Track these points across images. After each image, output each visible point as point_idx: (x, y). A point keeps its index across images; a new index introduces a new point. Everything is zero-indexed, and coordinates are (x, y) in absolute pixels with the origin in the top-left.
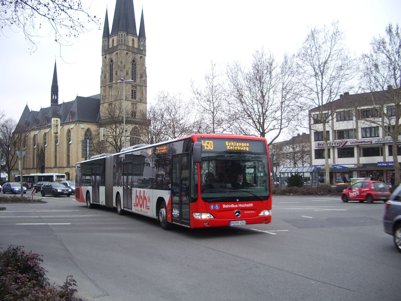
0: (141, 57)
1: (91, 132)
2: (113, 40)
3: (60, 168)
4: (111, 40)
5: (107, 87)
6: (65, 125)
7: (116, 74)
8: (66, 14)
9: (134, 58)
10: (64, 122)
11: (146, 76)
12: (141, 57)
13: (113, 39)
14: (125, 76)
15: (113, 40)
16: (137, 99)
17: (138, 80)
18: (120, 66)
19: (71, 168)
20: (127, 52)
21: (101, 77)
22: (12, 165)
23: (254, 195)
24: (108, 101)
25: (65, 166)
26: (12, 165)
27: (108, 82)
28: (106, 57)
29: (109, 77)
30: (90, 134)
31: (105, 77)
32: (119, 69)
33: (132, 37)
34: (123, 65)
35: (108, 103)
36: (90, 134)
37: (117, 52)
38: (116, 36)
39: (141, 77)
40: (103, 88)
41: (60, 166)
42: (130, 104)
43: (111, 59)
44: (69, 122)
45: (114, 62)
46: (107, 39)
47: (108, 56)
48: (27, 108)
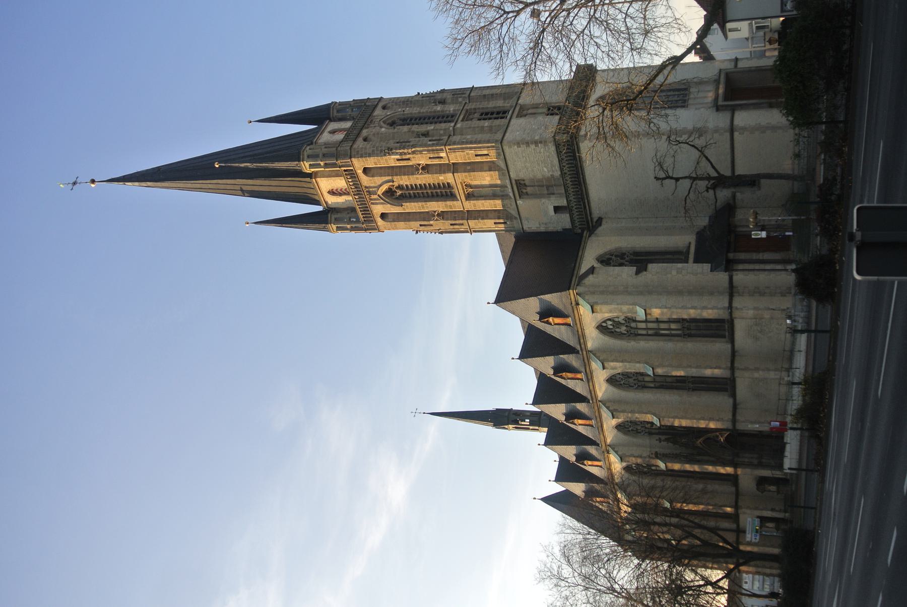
1: (612, 255)
2: (332, 192)
3: (736, 365)
4: (332, 200)
9: (384, 122)
11: (443, 91)
12: (384, 108)
13: (329, 192)
14: (430, 138)
15: (332, 192)
17: (451, 108)
18: (398, 157)
19: (736, 314)
20: (360, 139)
23: (751, 593)
24: (510, 197)
25: (729, 346)
34: (398, 144)
35: (518, 197)
39: (443, 102)
41: (729, 365)
42: (522, 121)
46: (333, 217)
47: (378, 209)
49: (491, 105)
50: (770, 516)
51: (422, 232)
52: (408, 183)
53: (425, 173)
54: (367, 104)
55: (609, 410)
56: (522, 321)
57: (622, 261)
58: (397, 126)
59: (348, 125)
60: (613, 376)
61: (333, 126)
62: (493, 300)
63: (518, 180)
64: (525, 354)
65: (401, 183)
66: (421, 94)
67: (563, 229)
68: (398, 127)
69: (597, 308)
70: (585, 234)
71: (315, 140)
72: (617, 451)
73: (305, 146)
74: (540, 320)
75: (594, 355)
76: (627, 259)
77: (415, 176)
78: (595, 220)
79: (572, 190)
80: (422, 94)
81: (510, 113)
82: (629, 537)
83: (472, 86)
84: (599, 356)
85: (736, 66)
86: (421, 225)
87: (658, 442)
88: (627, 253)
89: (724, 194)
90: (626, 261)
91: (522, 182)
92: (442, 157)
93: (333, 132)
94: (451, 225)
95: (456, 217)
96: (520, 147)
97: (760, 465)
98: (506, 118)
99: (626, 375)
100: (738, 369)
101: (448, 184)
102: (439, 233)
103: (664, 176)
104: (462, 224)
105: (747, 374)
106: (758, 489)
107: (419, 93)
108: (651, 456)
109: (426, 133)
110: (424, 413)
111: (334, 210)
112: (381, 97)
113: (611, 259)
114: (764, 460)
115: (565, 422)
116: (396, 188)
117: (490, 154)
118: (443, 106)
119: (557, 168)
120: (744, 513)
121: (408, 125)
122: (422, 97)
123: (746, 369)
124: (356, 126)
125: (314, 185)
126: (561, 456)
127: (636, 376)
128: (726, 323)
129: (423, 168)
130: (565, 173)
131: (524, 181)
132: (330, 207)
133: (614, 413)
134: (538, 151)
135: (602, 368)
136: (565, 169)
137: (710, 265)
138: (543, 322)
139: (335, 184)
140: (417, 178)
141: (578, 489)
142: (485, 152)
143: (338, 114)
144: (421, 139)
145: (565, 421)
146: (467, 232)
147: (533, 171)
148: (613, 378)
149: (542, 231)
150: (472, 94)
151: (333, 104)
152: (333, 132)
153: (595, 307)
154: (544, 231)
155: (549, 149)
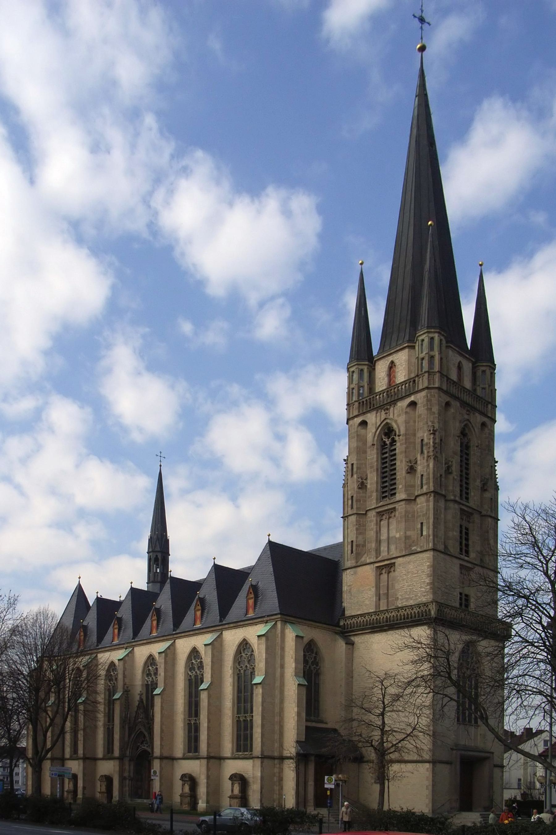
0: (483, 425)
1: (316, 654)
2: (392, 365)
4: (381, 368)
5: (372, 515)
6: (227, 629)
7: (412, 470)
8: (423, 8)
10: (357, 562)
13: (392, 362)
15: (392, 365)
16: (472, 555)
18: (426, 440)
20: (448, 399)
21: (344, 486)
22: (447, 648)
24: (377, 558)
26: (447, 648)
27: (377, 500)
28: (364, 423)
29: (377, 483)
30: (315, 658)
31: (362, 486)
32: (422, 452)
33: (459, 358)
36: (315, 658)
37: (412, 398)
38: (407, 350)
39: (484, 489)
40: (353, 519)
41: (212, 755)
43: (387, 423)
44: (245, 619)
45: (403, 431)
47: (373, 419)
48: (80, 593)
49: (474, 539)
50: (78, 785)
51: (345, 465)
52: (397, 451)
53: (358, 486)
54: (490, 406)
55: (166, 649)
56: (252, 568)
57: (310, 663)
58: (461, 439)
59: (467, 384)
60: (250, 646)
61: (467, 366)
62: (272, 539)
63: (395, 566)
64: (218, 570)
65: (398, 444)
66: (496, 464)
67: (344, 608)
68: (459, 440)
69: (264, 639)
70: (338, 629)
71: (452, 346)
72: (128, 656)
73: (445, 334)
74: (252, 585)
75: (219, 637)
76: (312, 667)
77: (404, 459)
78: (352, 638)
79: (355, 622)
80: (496, 466)
81: (466, 558)
82: (46, 664)
83: (499, 518)
84: (217, 641)
85: (496, 766)
86: (352, 464)
87: (139, 692)
88: (318, 668)
89: (372, 755)
90: (310, 667)
91: (392, 570)
92: (422, 487)
93: (460, 367)
94: (352, 497)
95: (360, 501)
96: (428, 568)
97: (122, 779)
98: (461, 554)
99: (251, 658)
100: (208, 762)
101: (395, 494)
102: (344, 484)
103: (386, 702)
104: (352, 508)
105: (204, 769)
106: (102, 776)
107: (497, 462)
108: (125, 686)
109: (450, 471)
110: (161, 466)
111: (373, 367)
112: (496, 421)
113: (313, 653)
114: (127, 781)
115: (197, 597)
116: (393, 438)
117: (422, 537)
118: (480, 488)
119: (405, 604)
120: (79, 765)
121: (461, 451)
122: (492, 466)
123: (208, 769)
124: (464, 393)
125: (401, 344)
126: (202, 584)
127: (250, 668)
128: (250, 753)
129: (362, 483)
130: (398, 612)
131: (394, 571)
132: (377, 364)
133: (163, 654)
134: (422, 585)
135: (159, 651)
136: (402, 611)
137: (304, 740)
138: (249, 588)
139: (401, 370)
140: (401, 461)
141: (91, 620)
142: (425, 533)
143: (481, 370)
144: (444, 465)
145: (199, 598)
146: (344, 514)
147: (403, 580)
148: (248, 646)
149: (343, 588)
150: (490, 520)
151: (493, 366)
152: (460, 367)
153: (264, 639)
154: (343, 590)
155: (424, 596)
